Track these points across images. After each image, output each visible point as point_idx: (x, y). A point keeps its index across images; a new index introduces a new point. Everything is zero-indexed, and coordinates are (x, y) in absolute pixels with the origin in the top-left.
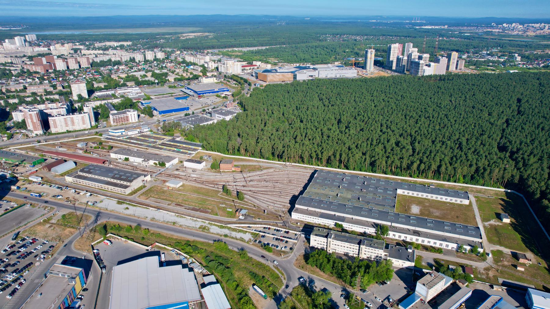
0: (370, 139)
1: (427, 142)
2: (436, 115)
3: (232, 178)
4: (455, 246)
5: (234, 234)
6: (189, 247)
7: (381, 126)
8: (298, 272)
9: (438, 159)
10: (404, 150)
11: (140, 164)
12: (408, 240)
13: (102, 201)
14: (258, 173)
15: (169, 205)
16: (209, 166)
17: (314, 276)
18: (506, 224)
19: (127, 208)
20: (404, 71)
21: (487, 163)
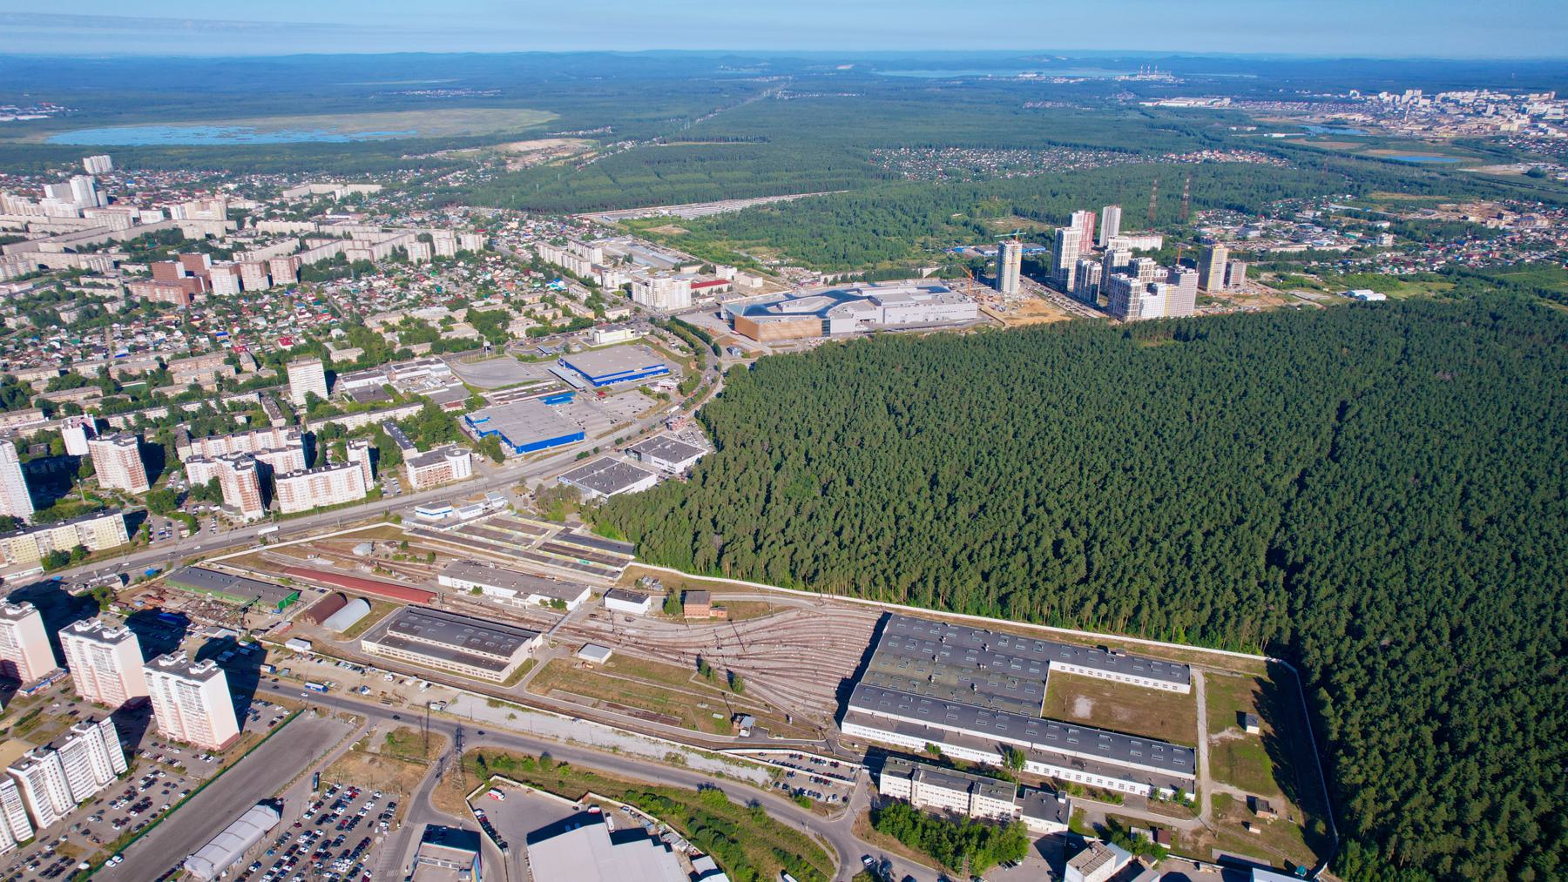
0: (1000, 536)
1: (1120, 544)
2: (1149, 463)
3: (712, 637)
4: (1146, 788)
5: (735, 770)
6: (651, 798)
7: (1026, 496)
8: (860, 846)
9: (1135, 590)
10: (1069, 567)
11: (508, 601)
12: (1062, 777)
13: (455, 701)
14: (766, 622)
15: (594, 706)
16: (659, 605)
17: (889, 854)
18: (1251, 736)
19: (512, 716)
20: (1094, 298)
21: (1234, 600)
